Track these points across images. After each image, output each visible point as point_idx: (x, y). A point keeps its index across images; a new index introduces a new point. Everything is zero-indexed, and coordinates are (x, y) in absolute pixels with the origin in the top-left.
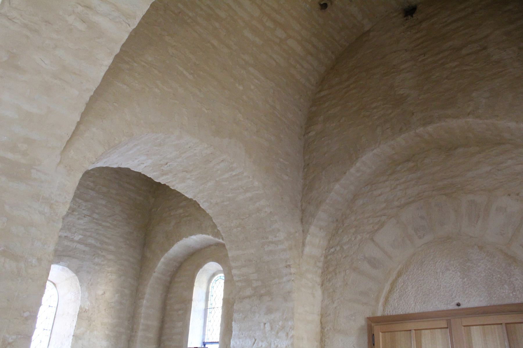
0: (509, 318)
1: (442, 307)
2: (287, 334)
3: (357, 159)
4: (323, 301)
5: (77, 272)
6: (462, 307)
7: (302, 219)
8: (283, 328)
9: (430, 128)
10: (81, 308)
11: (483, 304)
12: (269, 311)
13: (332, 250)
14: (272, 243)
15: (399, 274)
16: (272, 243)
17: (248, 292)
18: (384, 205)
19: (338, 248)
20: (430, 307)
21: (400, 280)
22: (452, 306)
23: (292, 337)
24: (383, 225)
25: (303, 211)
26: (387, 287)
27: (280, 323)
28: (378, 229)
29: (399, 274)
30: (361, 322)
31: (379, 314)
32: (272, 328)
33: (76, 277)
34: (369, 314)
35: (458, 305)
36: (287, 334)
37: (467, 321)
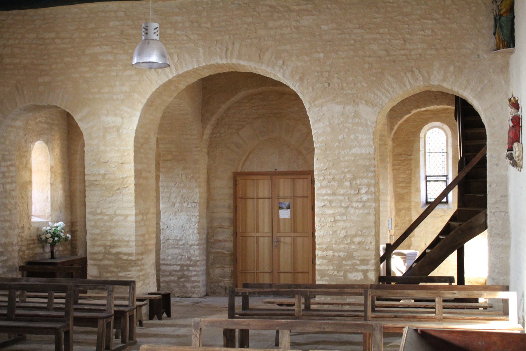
0: (294, 177)
1: (269, 170)
2: (196, 181)
3: (236, 93)
4: (208, 162)
5: (47, 143)
6: (278, 170)
7: (202, 120)
8: (193, 177)
9: (275, 88)
10: (51, 166)
11: (286, 170)
12: (184, 168)
13: (214, 135)
14: (189, 134)
15: (250, 153)
16: (189, 134)
17: (169, 157)
18: (245, 116)
19: (218, 135)
20: (263, 170)
21: (250, 155)
22: (273, 170)
23: (199, 182)
24: (244, 126)
25: (203, 116)
26: (244, 158)
27: (192, 175)
28: (241, 128)
29: (250, 153)
30: (230, 174)
31: (239, 170)
32: (186, 178)
33: (47, 147)
34: (234, 170)
35: (276, 169)
36: (196, 181)
37: (279, 177)
